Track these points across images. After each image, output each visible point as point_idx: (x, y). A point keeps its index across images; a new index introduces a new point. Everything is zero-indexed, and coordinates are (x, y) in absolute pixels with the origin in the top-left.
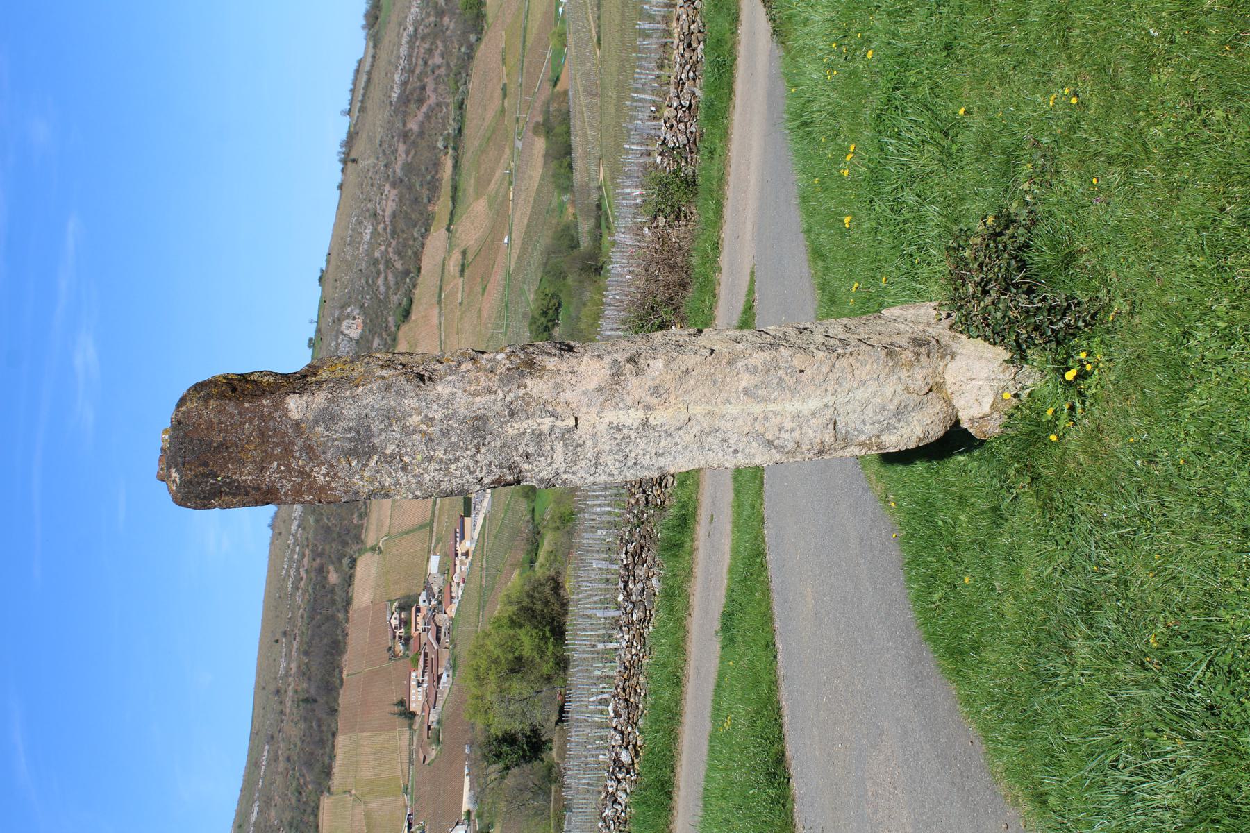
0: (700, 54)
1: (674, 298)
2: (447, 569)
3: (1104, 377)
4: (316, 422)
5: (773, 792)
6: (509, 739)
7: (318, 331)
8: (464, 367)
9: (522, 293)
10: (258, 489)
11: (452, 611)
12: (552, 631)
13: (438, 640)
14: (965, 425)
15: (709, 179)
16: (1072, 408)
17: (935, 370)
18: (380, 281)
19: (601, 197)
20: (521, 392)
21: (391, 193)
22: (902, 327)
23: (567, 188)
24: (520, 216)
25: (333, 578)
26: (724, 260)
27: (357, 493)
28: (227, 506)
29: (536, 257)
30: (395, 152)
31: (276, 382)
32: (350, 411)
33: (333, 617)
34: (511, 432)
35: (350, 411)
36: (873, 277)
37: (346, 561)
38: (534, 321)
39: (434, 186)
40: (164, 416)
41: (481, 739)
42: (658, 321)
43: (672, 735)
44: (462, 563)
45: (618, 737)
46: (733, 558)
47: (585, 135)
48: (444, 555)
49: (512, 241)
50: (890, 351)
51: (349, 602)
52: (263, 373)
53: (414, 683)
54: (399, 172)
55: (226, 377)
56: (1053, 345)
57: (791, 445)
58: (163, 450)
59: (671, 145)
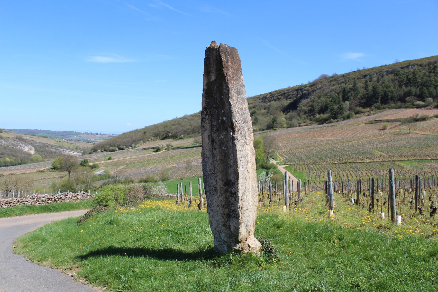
0: (4, 207)
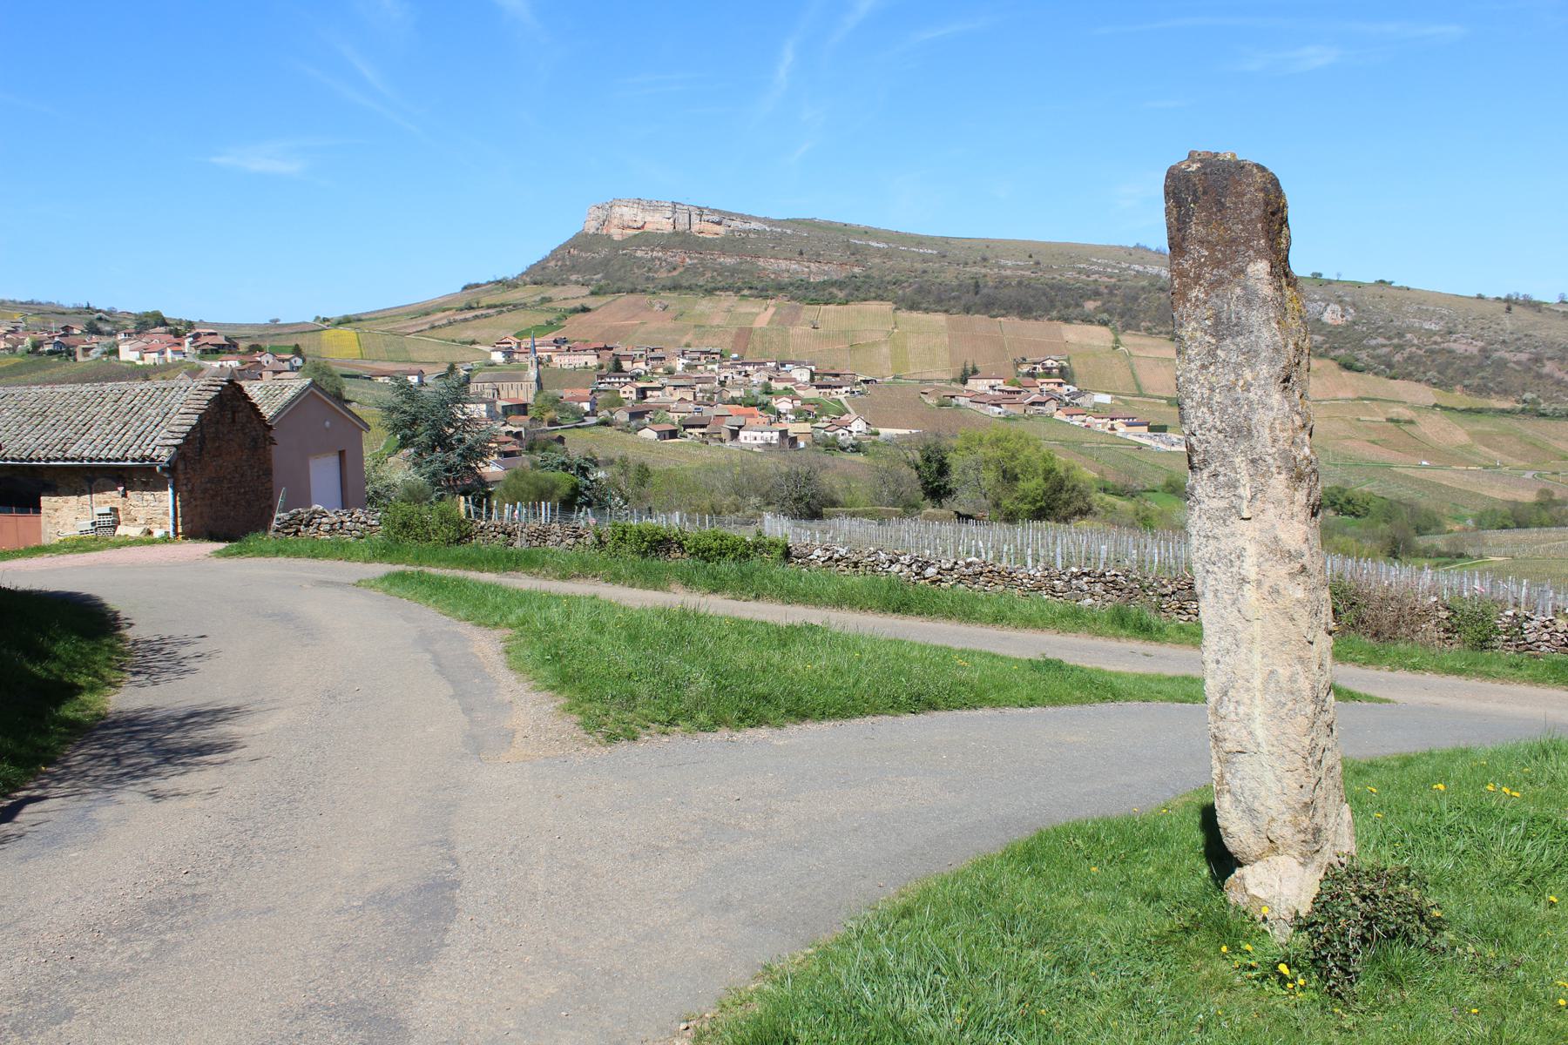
1: (1362, 625)
2: (1098, 411)
3: (1279, 998)
4: (1245, 288)
5: (903, 698)
6: (943, 470)
7: (1330, 282)
8: (1297, 418)
9: (1370, 479)
10: (1183, 240)
11: (1060, 416)
12: (1041, 508)
13: (1033, 404)
14: (1238, 871)
15: (1488, 662)
16: (1251, 968)
17: (1290, 847)
18: (1381, 340)
19: (1470, 558)
20: (1274, 470)
21: (1474, 349)
22: (1332, 820)
23: (1480, 523)
24: (1450, 477)
25: (1090, 305)
26: (1402, 675)
27: (1181, 325)
28: (1168, 213)
29: (1406, 493)
30: (1519, 350)
31: (1281, 250)
32: (1256, 317)
33: (1053, 307)
34: (1237, 460)
35: (1256, 317)
36: (1381, 807)
37: (1105, 316)
38: (1341, 491)
39: (1482, 390)
40: (1248, 154)
41: (943, 444)
42: (1340, 608)
43: (949, 615)
44: (1104, 425)
45: (948, 566)
46: (1110, 673)
47: (1539, 542)
48: (1112, 408)
49: (1422, 468)
50: (1308, 806)
51: (1067, 320)
52: (1288, 239)
53: (993, 382)
54: (1496, 355)
55: (1285, 206)
56: (1311, 956)
57: (1222, 712)
58: (1217, 154)
59: (1525, 625)
